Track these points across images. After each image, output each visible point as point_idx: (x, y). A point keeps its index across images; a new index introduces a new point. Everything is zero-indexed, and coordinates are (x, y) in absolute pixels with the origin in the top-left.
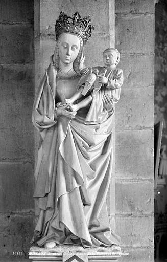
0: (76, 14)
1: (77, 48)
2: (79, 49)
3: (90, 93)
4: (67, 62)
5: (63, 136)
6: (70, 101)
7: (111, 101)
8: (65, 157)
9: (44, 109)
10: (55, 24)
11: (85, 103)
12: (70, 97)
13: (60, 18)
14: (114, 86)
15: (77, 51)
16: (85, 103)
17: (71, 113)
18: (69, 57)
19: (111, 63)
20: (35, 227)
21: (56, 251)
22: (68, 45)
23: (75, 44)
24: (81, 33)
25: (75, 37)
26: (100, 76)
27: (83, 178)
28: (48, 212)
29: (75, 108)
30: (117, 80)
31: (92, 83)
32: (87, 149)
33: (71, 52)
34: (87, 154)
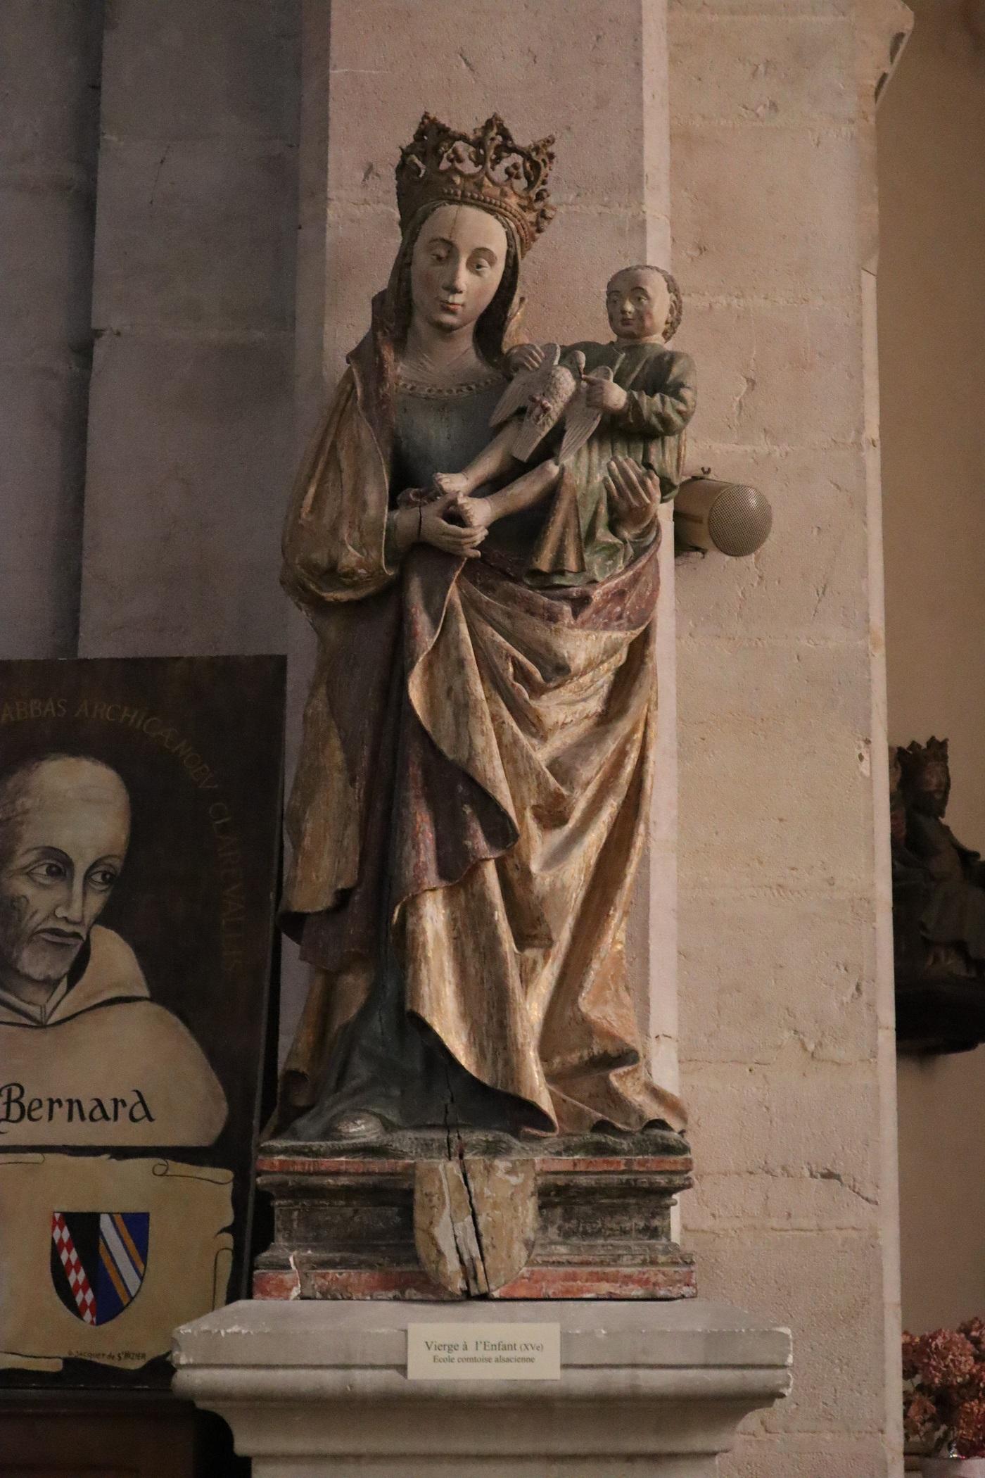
0: (489, 124)
1: (492, 263)
2: (501, 265)
3: (549, 448)
4: (448, 319)
5: (425, 636)
6: (456, 484)
7: (643, 484)
8: (434, 726)
9: (562, 541)
10: (396, 160)
11: (525, 491)
12: (458, 467)
13: (419, 135)
14: (654, 420)
15: (494, 275)
16: (525, 491)
17: (463, 531)
18: (458, 299)
19: (642, 328)
20: (444, 897)
21: (591, 508)
22: (451, 250)
23: (482, 245)
24: (513, 201)
25: (490, 219)
26: (592, 376)
27: (515, 821)
28: (35, 1117)
29: (481, 513)
30: (668, 399)
31: (556, 407)
32: (537, 691)
33: (465, 278)
34: (602, 552)
